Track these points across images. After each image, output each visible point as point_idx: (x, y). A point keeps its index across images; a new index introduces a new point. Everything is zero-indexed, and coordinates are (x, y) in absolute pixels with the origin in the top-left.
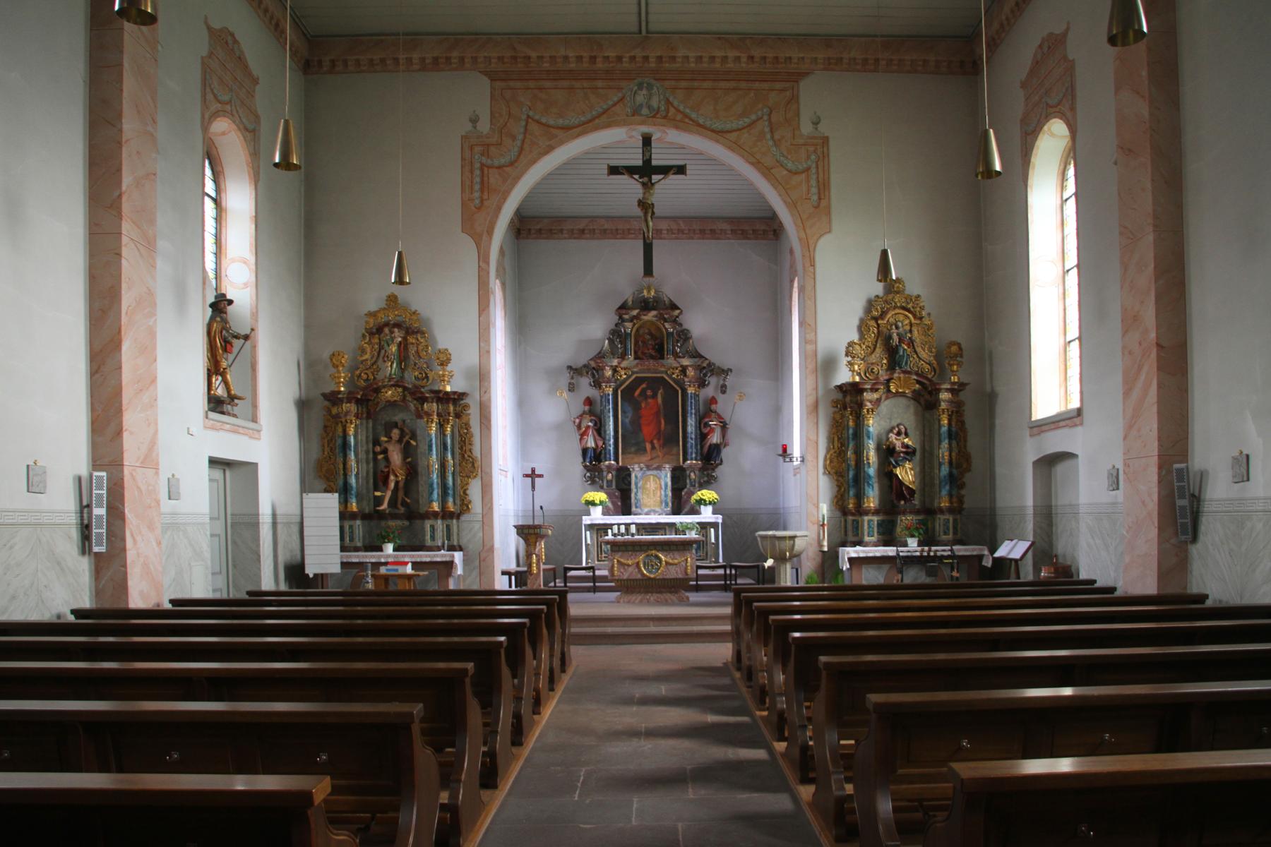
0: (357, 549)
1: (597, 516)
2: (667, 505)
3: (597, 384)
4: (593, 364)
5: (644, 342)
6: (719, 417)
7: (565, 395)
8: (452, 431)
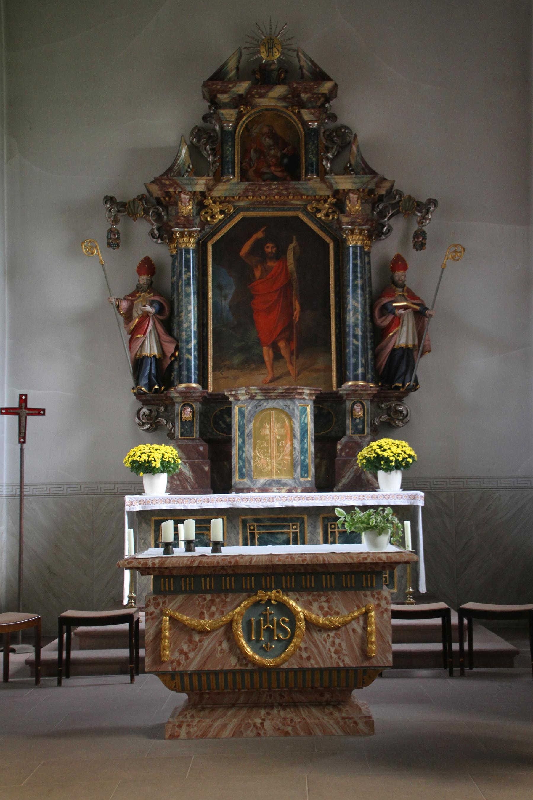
1: (157, 492)
2: (305, 470)
3: (164, 233)
4: (156, 191)
5: (260, 152)
6: (411, 296)
7: (98, 252)
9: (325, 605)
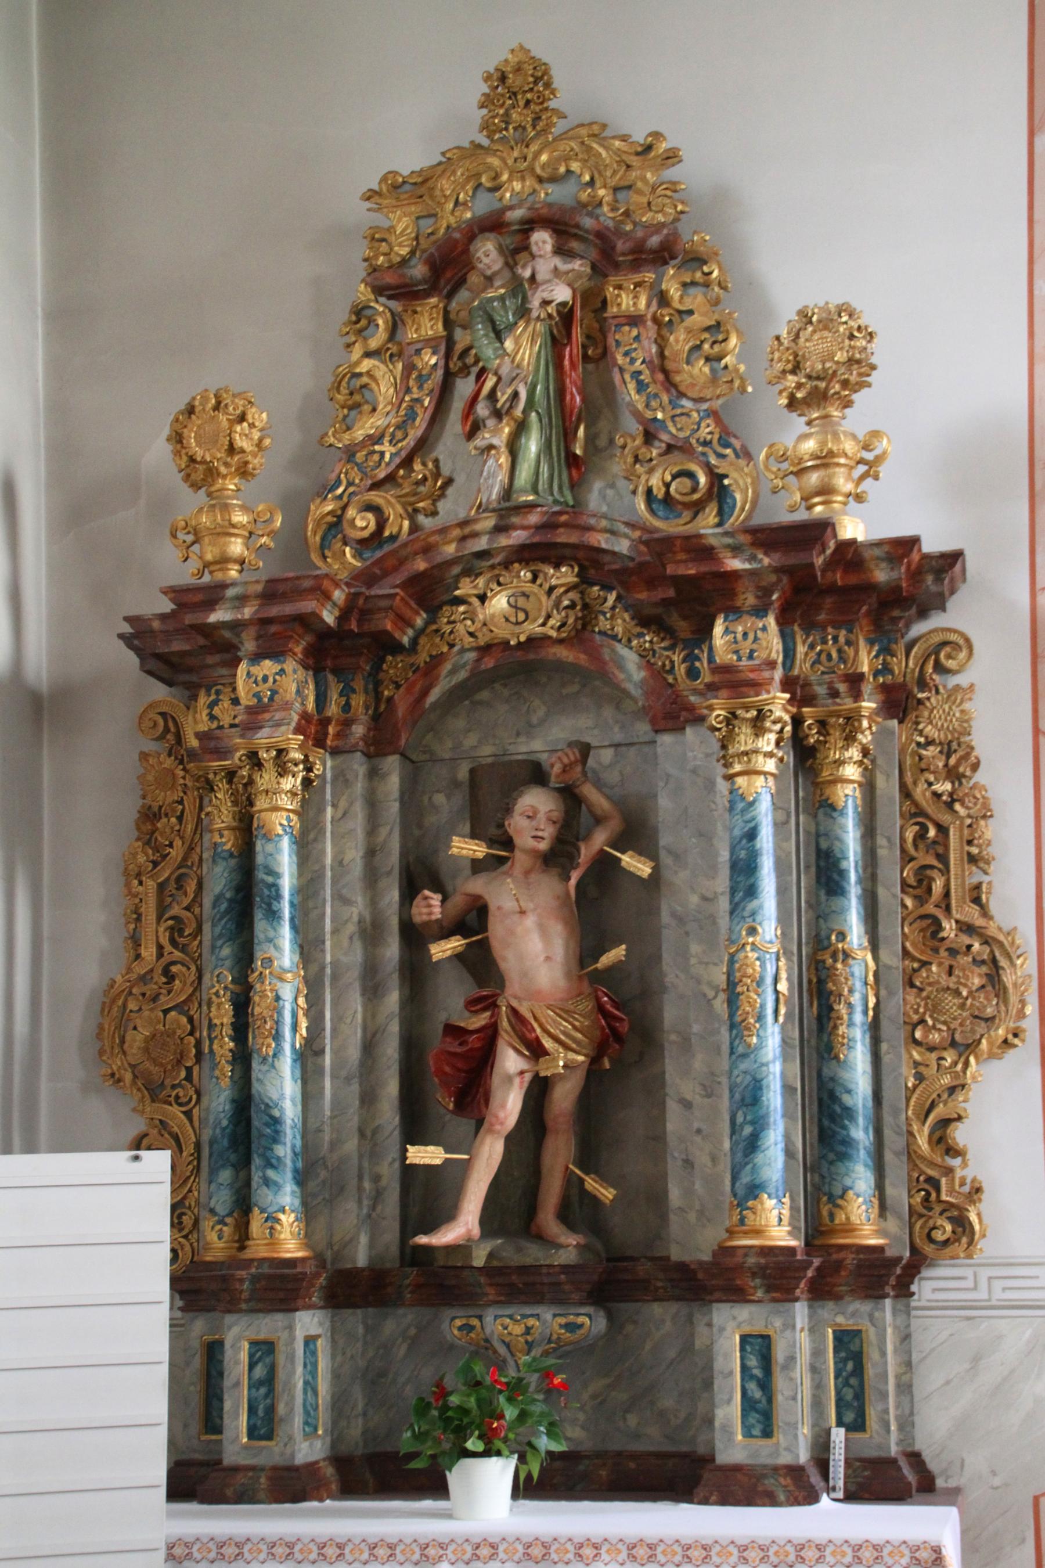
0: (291, 1486)
8: (869, 787)
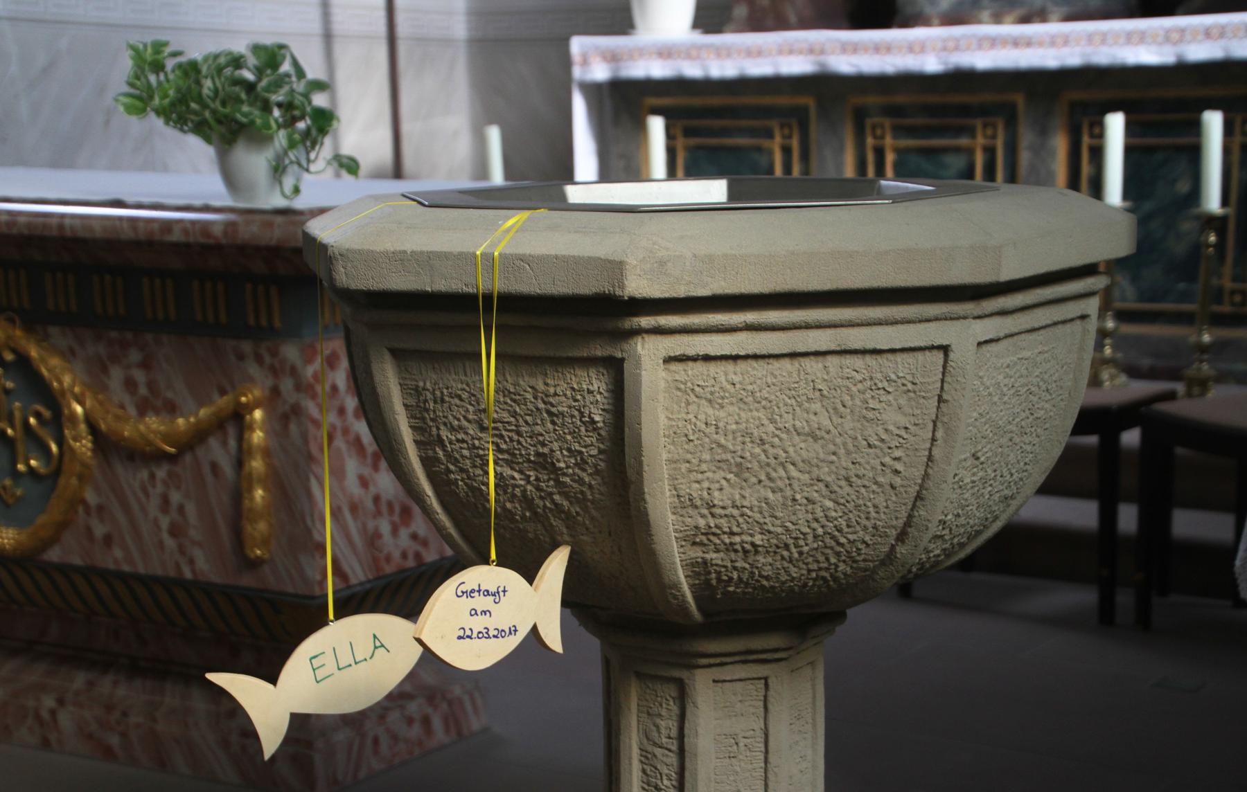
9: (140, 376)
